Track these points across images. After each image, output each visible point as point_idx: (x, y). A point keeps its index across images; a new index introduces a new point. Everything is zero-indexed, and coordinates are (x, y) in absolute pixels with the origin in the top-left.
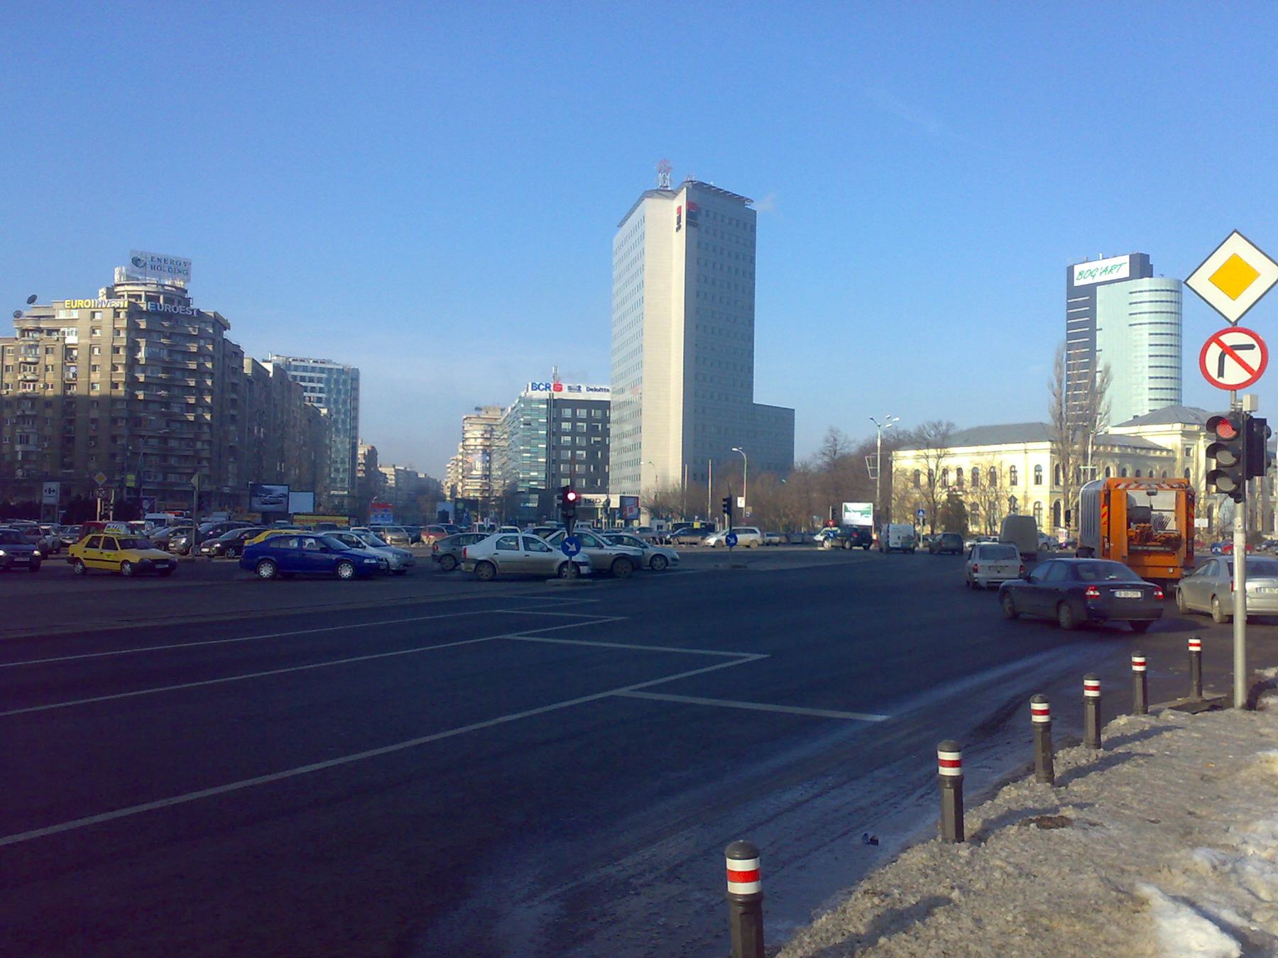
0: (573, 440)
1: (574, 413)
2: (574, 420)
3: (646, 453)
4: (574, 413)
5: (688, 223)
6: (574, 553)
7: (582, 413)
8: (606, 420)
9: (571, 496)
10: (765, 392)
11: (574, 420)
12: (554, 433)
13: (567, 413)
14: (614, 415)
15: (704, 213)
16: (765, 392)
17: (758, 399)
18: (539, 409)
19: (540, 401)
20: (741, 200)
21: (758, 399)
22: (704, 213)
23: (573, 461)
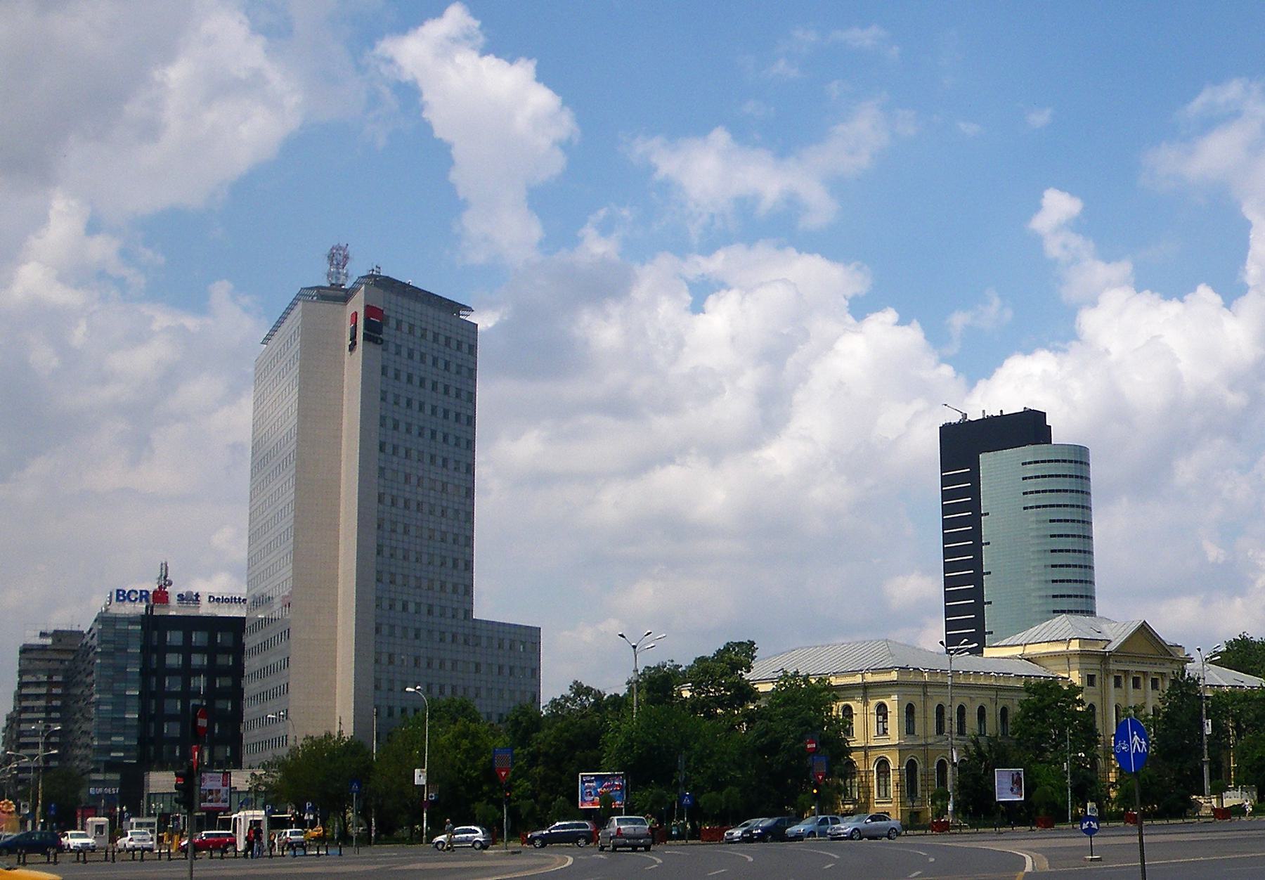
0: (187, 660)
1: (187, 638)
2: (187, 649)
3: (296, 699)
4: (187, 638)
5: (367, 338)
6: (464, 735)
7: (198, 638)
8: (238, 650)
9: (202, 722)
10: (492, 601)
11: (187, 649)
12: (151, 672)
13: (174, 637)
14: (250, 641)
15: (393, 323)
16: (492, 601)
17: (479, 613)
18: (128, 633)
19: (130, 620)
20: (455, 308)
21: (479, 613)
22: (393, 323)
23: (187, 693)
